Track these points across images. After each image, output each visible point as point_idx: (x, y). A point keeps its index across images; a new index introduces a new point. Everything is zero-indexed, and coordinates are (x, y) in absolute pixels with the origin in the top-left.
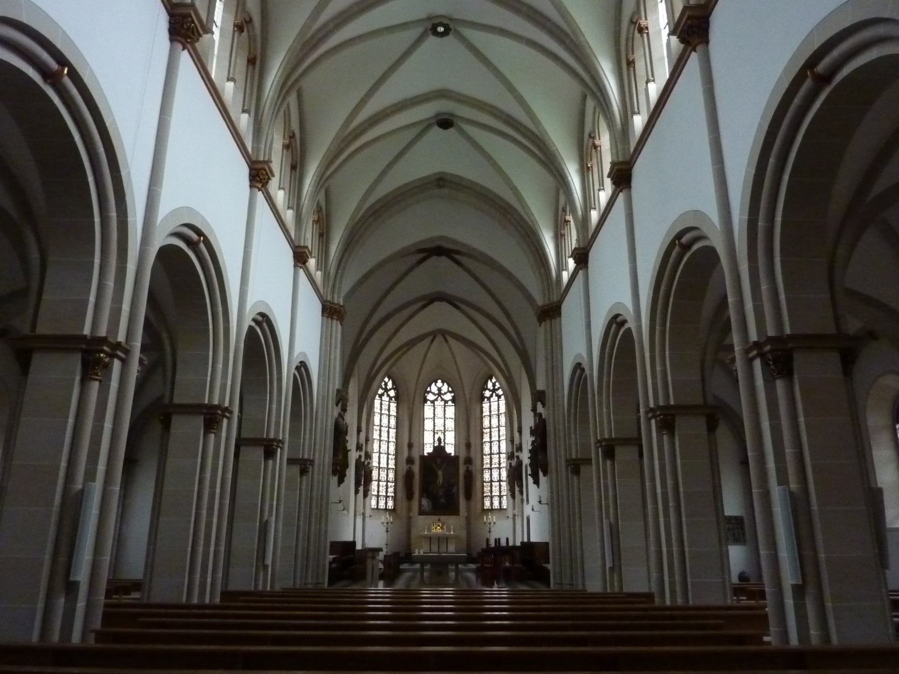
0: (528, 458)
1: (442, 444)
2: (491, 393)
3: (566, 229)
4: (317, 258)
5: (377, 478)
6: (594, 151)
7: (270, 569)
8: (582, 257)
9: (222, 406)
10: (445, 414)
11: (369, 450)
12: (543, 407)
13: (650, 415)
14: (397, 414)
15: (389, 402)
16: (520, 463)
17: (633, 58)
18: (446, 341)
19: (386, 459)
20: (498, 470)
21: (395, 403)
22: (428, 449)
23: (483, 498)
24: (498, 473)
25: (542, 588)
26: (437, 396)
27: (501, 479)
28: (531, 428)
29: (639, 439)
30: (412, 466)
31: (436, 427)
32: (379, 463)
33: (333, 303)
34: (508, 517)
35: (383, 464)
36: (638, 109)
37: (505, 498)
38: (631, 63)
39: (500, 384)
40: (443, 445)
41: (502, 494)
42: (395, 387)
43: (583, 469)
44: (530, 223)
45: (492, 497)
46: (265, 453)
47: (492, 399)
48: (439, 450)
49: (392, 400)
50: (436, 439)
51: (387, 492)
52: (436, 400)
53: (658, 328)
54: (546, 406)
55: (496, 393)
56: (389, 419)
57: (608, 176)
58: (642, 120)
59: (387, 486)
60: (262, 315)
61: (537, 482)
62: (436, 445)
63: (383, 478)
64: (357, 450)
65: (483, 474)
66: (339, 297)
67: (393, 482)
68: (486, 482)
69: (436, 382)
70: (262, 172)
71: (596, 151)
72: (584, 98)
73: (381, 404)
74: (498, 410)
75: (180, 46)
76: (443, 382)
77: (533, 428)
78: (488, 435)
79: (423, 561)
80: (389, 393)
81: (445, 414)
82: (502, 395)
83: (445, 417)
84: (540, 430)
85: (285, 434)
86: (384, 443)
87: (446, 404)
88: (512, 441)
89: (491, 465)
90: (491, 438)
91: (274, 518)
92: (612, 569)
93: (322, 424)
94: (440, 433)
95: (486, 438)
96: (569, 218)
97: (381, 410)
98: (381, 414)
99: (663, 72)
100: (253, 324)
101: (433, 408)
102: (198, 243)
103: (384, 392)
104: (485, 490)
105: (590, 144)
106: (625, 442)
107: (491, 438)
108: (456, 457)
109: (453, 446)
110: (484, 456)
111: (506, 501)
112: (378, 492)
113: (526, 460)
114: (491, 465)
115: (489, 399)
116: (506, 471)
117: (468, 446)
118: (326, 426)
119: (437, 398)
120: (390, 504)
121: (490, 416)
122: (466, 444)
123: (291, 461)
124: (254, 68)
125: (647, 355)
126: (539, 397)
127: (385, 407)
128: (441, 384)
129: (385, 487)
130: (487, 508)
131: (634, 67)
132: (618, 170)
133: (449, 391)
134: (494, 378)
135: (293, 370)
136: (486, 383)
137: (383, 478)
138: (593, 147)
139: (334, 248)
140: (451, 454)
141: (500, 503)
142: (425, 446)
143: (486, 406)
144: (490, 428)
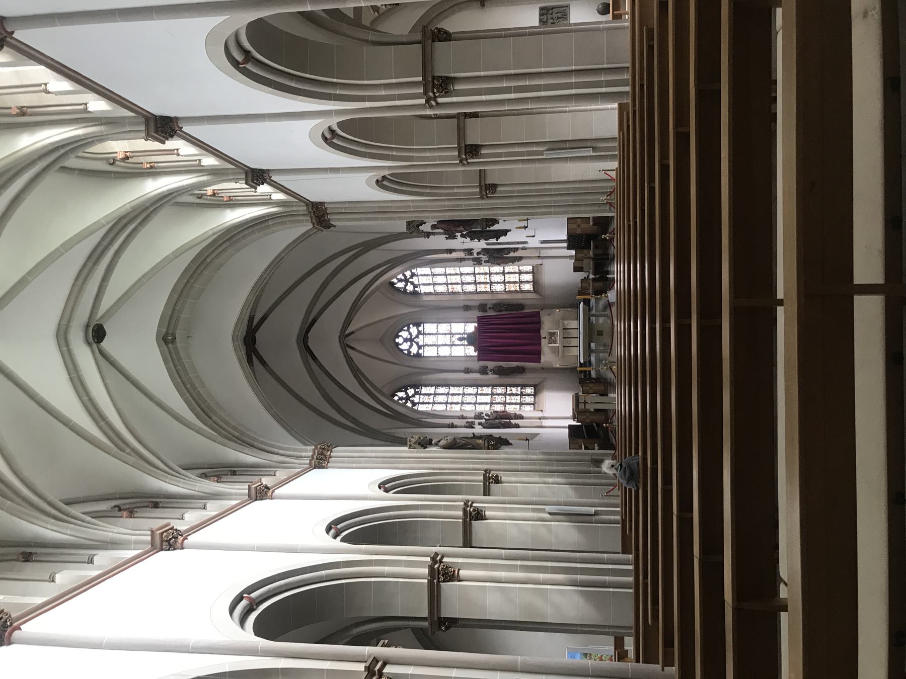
0: (479, 241)
1: (466, 336)
2: (409, 284)
3: (222, 195)
4: (261, 477)
5: (502, 405)
6: (130, 160)
7: (599, 509)
8: (257, 176)
9: (430, 564)
10: (433, 334)
11: (473, 415)
12: (425, 223)
13: (433, 103)
14: (434, 386)
15: (420, 394)
16: (485, 251)
17: (16, 108)
18: (352, 333)
19: (482, 396)
20: (492, 275)
21: (421, 388)
22: (471, 351)
23: (522, 292)
24: (495, 275)
25: (614, 225)
26: (413, 343)
27: (501, 272)
28: (447, 238)
29: (457, 116)
30: (489, 369)
31: (447, 344)
32: (486, 404)
33: (313, 456)
34: (541, 265)
35: (487, 399)
36: (81, 104)
37: (521, 268)
38: (23, 111)
39: (399, 274)
40: (466, 335)
41: (518, 271)
42: (405, 388)
43: (490, 181)
44: (216, 236)
45: (521, 282)
46: (477, 519)
47: (416, 283)
48: (471, 339)
49: (418, 392)
50: (459, 343)
51: (517, 395)
52: (417, 343)
53: (338, 92)
54: (425, 220)
55: (409, 279)
56: (439, 394)
57: (164, 143)
58: (95, 100)
59: (510, 395)
60: (328, 530)
61: (505, 232)
62: (466, 343)
63: (502, 399)
64: (474, 428)
65: (497, 293)
66: (306, 451)
67: (507, 389)
68: (505, 289)
69: (398, 344)
70: (165, 536)
71: (132, 157)
72: (64, 168)
73: (423, 403)
74: (428, 275)
75: (16, 633)
76: (398, 336)
77: (447, 236)
78: (455, 286)
79: (588, 351)
80: (410, 395)
81: (433, 334)
82: (411, 271)
83: (437, 334)
84: (450, 227)
85: (458, 500)
86: (465, 399)
87: (422, 332)
88: (461, 260)
89: (486, 283)
90: (457, 284)
91: (546, 507)
92: (595, 149)
93: (446, 463)
94: (453, 339)
95: (458, 288)
96: (209, 190)
97: (429, 403)
98: (434, 403)
99: (38, 73)
100: (339, 538)
101: (426, 347)
102: (250, 599)
103: (410, 400)
104: (514, 290)
105: (122, 164)
106: (461, 132)
107: (457, 284)
108: (480, 320)
109: (468, 324)
110: (478, 291)
111: (525, 267)
112: (516, 404)
113: (478, 245)
114: (486, 283)
115: (415, 286)
116: (493, 267)
117: (467, 308)
118: (448, 458)
119: (415, 342)
120: (529, 390)
121: (434, 284)
122: (465, 311)
123: (487, 492)
124: (36, 553)
125: (368, 104)
126: (414, 228)
127: (426, 399)
128: (400, 338)
129: (512, 396)
130: (532, 286)
131: (27, 107)
132: (156, 132)
133: (408, 330)
134: (392, 281)
135: (390, 494)
136: (398, 289)
137: (502, 399)
138: (127, 161)
139: (248, 458)
140: (475, 327)
141: (527, 273)
142: (468, 355)
143: (423, 289)
144: (447, 284)
